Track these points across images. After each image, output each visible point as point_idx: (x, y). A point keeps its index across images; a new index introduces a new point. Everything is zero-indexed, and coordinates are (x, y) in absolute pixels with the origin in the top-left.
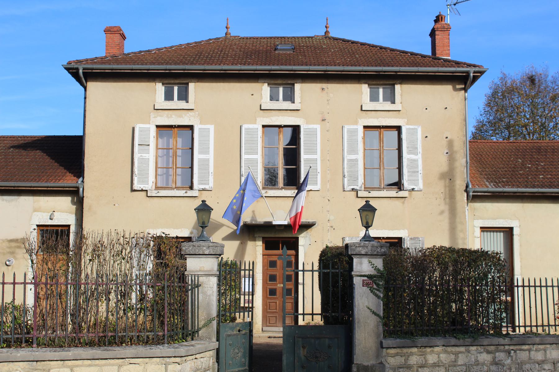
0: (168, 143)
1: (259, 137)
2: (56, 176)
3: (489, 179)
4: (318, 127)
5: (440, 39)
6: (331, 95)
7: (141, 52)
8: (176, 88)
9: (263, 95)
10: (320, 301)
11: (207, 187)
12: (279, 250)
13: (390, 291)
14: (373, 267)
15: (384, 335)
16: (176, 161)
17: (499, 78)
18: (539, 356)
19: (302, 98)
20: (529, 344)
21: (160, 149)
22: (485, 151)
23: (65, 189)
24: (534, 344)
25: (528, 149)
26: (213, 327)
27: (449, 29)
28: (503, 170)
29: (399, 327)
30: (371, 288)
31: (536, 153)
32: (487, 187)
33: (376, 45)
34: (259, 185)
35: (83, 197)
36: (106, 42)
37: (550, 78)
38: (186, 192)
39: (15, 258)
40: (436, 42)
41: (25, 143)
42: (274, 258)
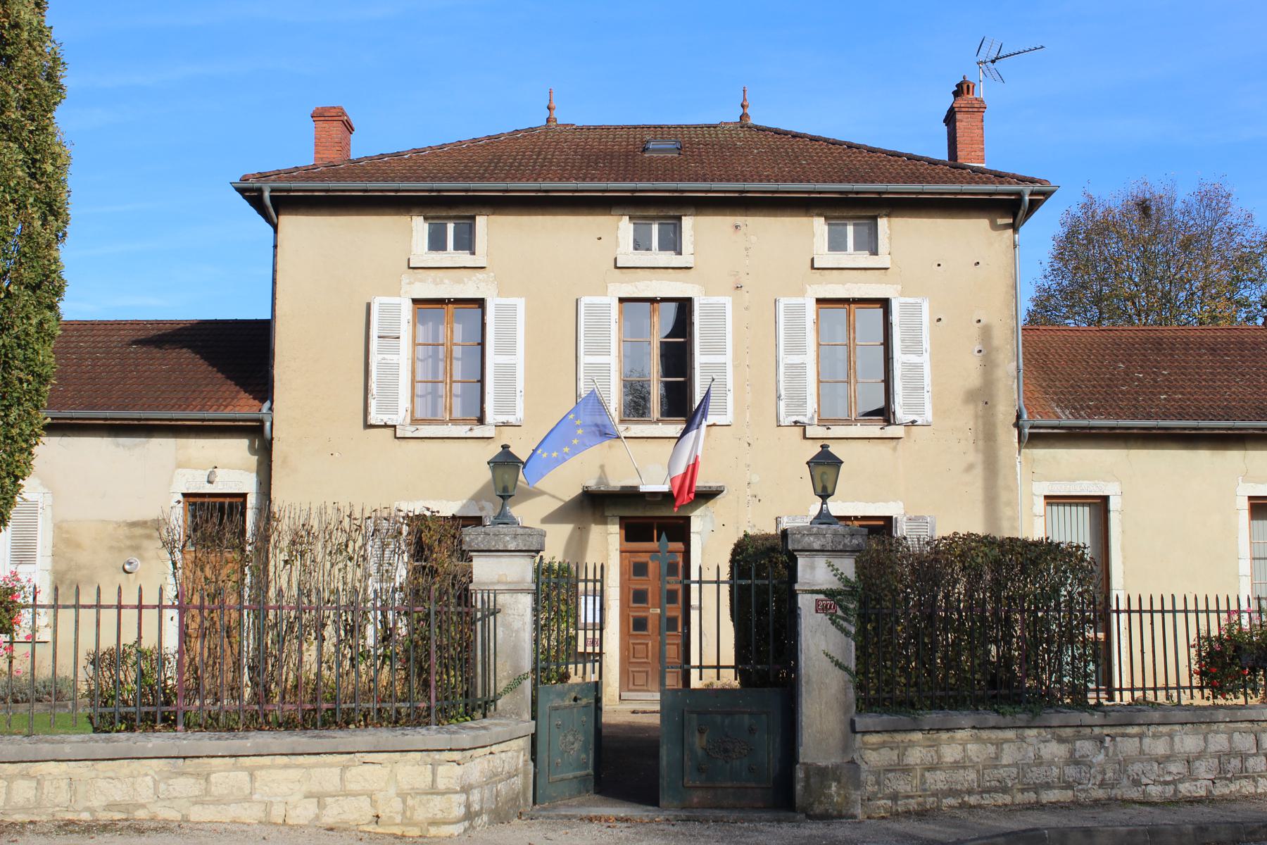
2: (219, 399)
3: (1062, 402)
4: (727, 301)
6: (753, 239)
8: (451, 227)
9: (620, 239)
11: (512, 419)
13: (870, 621)
14: (835, 575)
15: (857, 707)
16: (451, 369)
17: (1081, 205)
18: (1160, 747)
19: (695, 244)
20: (1139, 725)
21: (420, 344)
24: (1149, 725)
25: (1137, 343)
26: (524, 693)
27: (981, 110)
29: (888, 692)
30: (832, 615)
32: (1059, 417)
34: (613, 415)
35: (272, 439)
37: (1179, 205)
38: (471, 430)
39: (142, 558)
41: (159, 335)
42: (642, 558)
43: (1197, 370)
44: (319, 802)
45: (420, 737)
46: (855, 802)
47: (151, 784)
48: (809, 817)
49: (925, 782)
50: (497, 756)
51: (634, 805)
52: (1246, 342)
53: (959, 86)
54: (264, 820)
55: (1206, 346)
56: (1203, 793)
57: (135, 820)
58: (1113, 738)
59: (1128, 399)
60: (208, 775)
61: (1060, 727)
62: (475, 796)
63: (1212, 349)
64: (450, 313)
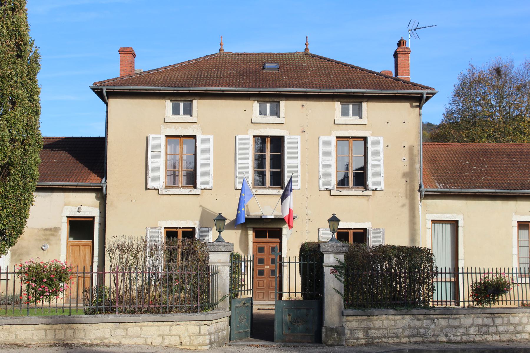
0: (175, 149)
1: (250, 145)
2: (82, 176)
3: (440, 180)
4: (299, 137)
5: (401, 61)
6: (310, 111)
7: (151, 71)
8: (182, 104)
9: (254, 110)
10: (300, 282)
11: (208, 187)
12: (267, 238)
13: (349, 276)
14: (337, 261)
15: (344, 307)
16: (182, 165)
17: (468, 70)
18: (456, 323)
19: (285, 113)
21: (169, 154)
22: (439, 153)
23: (91, 187)
24: (452, 314)
25: (476, 151)
26: (227, 301)
27: (409, 53)
28: (452, 172)
29: (356, 302)
30: (336, 274)
31: (483, 155)
32: (437, 188)
33: (348, 64)
34: (250, 185)
35: (106, 194)
36: (120, 61)
37: (515, 70)
38: (191, 191)
39: (50, 244)
40: (398, 64)
41: (49, 144)
42: (262, 245)
43: (500, 165)
44: (162, 338)
45: (195, 316)
46: (343, 340)
47: (109, 332)
48: (327, 345)
49: (368, 334)
50: (219, 323)
51: (265, 341)
52: (524, 151)
53: (400, 42)
54: (145, 343)
55: (506, 153)
56: (472, 340)
57: (104, 343)
58: (438, 319)
59: (468, 179)
60: (127, 328)
61: (418, 315)
62: (213, 337)
63: (509, 155)
64: (181, 141)
